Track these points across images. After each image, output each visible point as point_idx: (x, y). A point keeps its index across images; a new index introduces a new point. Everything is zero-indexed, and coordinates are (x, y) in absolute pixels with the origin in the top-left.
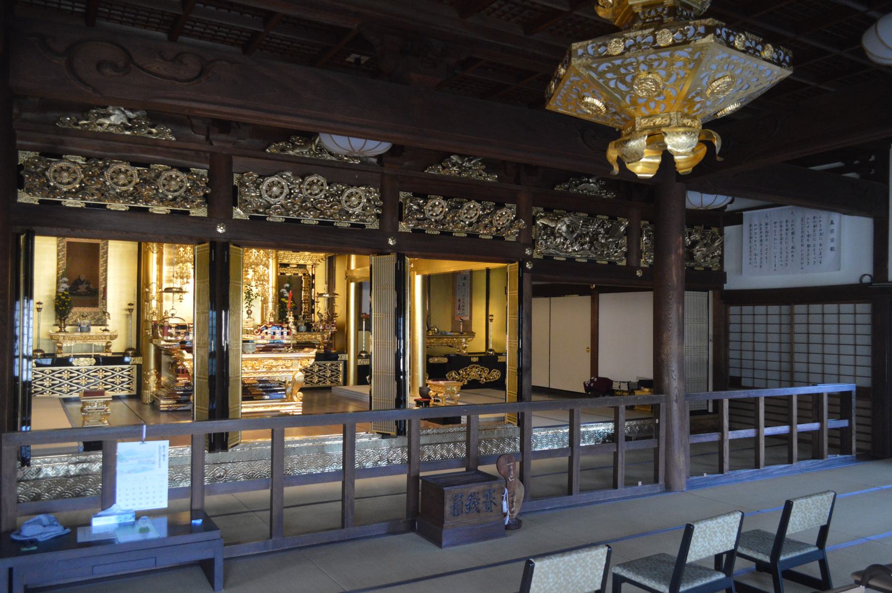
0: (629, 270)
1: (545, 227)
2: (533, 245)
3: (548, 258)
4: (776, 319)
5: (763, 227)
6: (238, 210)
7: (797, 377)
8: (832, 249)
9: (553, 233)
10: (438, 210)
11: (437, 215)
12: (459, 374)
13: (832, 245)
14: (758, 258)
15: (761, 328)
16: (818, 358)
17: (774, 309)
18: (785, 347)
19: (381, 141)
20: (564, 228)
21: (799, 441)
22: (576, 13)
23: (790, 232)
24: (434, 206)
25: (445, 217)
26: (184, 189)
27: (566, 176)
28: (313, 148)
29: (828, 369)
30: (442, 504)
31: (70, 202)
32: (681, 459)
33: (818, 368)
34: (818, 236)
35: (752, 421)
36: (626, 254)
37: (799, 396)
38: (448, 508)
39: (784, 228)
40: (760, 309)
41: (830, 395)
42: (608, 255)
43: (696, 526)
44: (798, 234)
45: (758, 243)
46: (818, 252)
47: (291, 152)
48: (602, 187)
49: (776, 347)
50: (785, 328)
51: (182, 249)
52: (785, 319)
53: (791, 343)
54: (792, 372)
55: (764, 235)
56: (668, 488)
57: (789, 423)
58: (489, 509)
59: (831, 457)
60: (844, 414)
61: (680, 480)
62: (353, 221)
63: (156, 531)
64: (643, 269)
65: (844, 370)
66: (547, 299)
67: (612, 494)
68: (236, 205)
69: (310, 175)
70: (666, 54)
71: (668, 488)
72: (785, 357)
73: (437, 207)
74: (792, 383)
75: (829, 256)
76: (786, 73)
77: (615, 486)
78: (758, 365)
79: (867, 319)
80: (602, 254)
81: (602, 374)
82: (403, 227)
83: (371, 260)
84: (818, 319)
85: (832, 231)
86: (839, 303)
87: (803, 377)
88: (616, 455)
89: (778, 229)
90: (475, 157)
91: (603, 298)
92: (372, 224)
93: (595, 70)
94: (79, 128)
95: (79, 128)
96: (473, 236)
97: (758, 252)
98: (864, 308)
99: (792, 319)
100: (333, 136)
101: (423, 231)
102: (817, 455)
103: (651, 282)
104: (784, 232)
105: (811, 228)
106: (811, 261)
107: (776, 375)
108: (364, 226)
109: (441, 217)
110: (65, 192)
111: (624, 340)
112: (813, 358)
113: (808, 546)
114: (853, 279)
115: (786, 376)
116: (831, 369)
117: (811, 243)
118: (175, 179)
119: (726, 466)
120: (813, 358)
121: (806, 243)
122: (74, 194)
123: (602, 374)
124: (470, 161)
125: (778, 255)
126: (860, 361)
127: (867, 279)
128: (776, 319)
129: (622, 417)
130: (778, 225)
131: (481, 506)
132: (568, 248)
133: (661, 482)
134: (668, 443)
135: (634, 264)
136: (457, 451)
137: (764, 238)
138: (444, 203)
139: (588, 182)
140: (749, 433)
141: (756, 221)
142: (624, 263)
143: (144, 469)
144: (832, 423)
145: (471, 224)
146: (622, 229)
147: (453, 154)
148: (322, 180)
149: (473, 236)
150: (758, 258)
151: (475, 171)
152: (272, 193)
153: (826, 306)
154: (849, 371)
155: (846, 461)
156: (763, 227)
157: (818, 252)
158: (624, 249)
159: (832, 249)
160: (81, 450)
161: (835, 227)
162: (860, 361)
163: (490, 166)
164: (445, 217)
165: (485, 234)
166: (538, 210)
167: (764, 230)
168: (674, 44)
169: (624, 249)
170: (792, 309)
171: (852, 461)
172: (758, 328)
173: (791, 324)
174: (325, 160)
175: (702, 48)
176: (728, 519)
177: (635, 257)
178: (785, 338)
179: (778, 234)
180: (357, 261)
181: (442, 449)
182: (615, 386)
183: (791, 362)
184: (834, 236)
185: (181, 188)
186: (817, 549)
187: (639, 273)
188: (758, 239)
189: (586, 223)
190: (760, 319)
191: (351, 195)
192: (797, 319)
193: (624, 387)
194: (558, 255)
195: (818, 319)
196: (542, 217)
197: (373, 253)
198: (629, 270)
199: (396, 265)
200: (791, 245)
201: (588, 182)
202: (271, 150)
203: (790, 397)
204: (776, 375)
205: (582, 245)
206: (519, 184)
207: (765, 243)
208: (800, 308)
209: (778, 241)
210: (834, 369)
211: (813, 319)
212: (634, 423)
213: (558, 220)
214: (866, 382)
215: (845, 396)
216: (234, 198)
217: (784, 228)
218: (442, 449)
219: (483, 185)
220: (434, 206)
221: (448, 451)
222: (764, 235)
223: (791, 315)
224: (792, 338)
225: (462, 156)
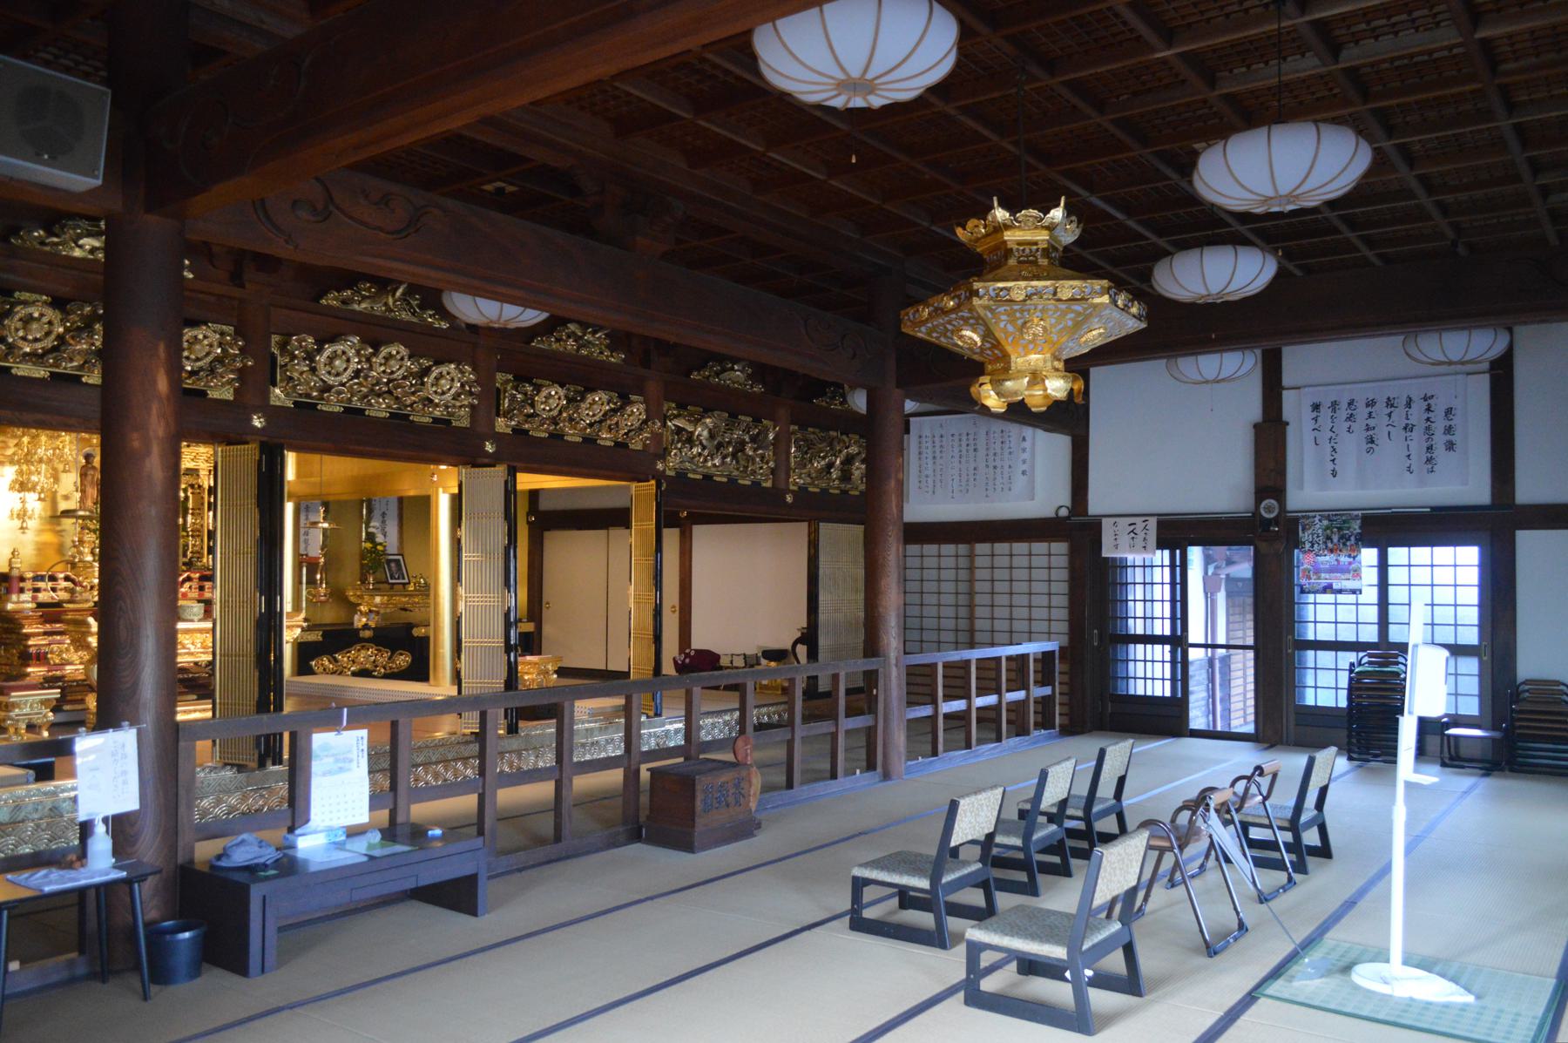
0: (776, 494)
1: (679, 430)
2: (663, 455)
3: (681, 475)
4: (951, 562)
5: (937, 439)
6: (277, 391)
7: (978, 637)
8: (1024, 473)
9: (690, 440)
10: (553, 403)
11: (198, 359)
12: (336, 660)
13: (1024, 467)
14: (930, 480)
15: (1021, 574)
16: (1005, 612)
17: (948, 549)
18: (963, 600)
19: (526, 306)
20: (705, 433)
21: (979, 720)
22: (833, 182)
23: (971, 448)
24: (549, 396)
25: (560, 413)
26: (53, 336)
27: (705, 358)
28: (391, 301)
29: (1017, 626)
30: (693, 797)
31: (23, 370)
32: (899, 738)
33: (1005, 625)
34: (1006, 455)
35: (993, 684)
36: (773, 471)
37: (946, 666)
38: (699, 804)
39: (964, 443)
40: (1020, 547)
41: (1009, 658)
42: (753, 472)
43: (962, 802)
44: (982, 452)
45: (930, 461)
46: (1006, 476)
47: (356, 307)
48: (749, 377)
49: (950, 599)
50: (963, 575)
51: (26, 439)
52: (963, 562)
53: (971, 594)
54: (972, 631)
55: (938, 449)
56: (886, 776)
57: (998, 691)
58: (738, 803)
59: (1036, 733)
60: (1046, 679)
61: (899, 762)
62: (437, 413)
63: (357, 851)
64: (793, 492)
65: (1036, 626)
66: (603, 532)
67: (834, 786)
68: (275, 385)
69: (388, 342)
70: (1063, 306)
71: (886, 776)
72: (963, 612)
73: (552, 398)
74: (972, 645)
75: (1020, 482)
76: (1143, 325)
77: (834, 776)
78: (927, 623)
79: (1063, 561)
80: (745, 471)
81: (698, 643)
82: (501, 425)
83: (459, 474)
84: (1005, 561)
85: (1024, 450)
86: (1409, 546)
87: (986, 637)
88: (790, 745)
89: (956, 444)
90: (601, 328)
91: (699, 531)
92: (462, 420)
93: (991, 311)
94: (47, 249)
95: (47, 249)
96: (589, 441)
97: (930, 472)
98: (1060, 548)
99: (972, 562)
100: (478, 299)
101: (526, 432)
102: (1021, 730)
103: (814, 509)
104: (964, 448)
105: (998, 445)
106: (999, 487)
107: (950, 637)
108: (449, 422)
109: (555, 413)
110: (26, 354)
111: (746, 589)
112: (998, 612)
113: (1107, 800)
114: (1048, 512)
115: (963, 637)
116: (1020, 626)
117: (998, 463)
118: (38, 320)
119: (941, 747)
120: (998, 612)
121: (991, 464)
122: (36, 358)
123: (698, 643)
124: (594, 333)
125: (957, 478)
126: (1056, 614)
127: (1064, 512)
128: (951, 562)
129: (751, 699)
130: (956, 438)
131: (731, 799)
132: (706, 461)
133: (879, 769)
134: (886, 720)
135: (782, 486)
136: (469, 772)
137: (938, 454)
138: (562, 392)
139: (732, 369)
140: (926, 711)
141: (927, 432)
142: (768, 484)
143: (341, 770)
144: (1039, 692)
145: (591, 425)
146: (771, 436)
147: (571, 321)
148: (404, 351)
149: (589, 441)
150: (930, 480)
151: (596, 347)
152: (338, 369)
153: (1015, 545)
154: (1043, 626)
155: (1050, 737)
156: (937, 439)
157: (1006, 476)
158: (772, 464)
159: (1024, 473)
160: (32, 779)
161: (1027, 445)
162: (1056, 614)
163: (617, 340)
164: (560, 413)
165: (572, 435)
166: (670, 407)
167: (938, 444)
168: (1072, 300)
169: (772, 464)
170: (972, 550)
171: (1055, 737)
172: (927, 574)
173: (971, 569)
174: (401, 321)
175: (1096, 306)
176: (989, 793)
177: (783, 476)
178: (963, 587)
179: (956, 450)
180: (299, 464)
181: (446, 770)
182: (724, 662)
183: (971, 618)
184: (1025, 456)
185: (48, 334)
186: (980, 865)
187: (789, 499)
188: (930, 456)
189: (729, 429)
190: (931, 562)
191: (441, 376)
192: (979, 562)
193: (739, 662)
194: (694, 472)
195: (1024, 561)
196: (676, 417)
197: (465, 464)
198: (776, 494)
199: (260, 462)
200: (972, 465)
201: (732, 369)
202: (331, 300)
203: (968, 662)
204: (950, 637)
205: (724, 457)
206: (242, 286)
207: (938, 461)
208: (982, 548)
209: (956, 459)
210: (1023, 626)
211: (1017, 561)
212: (772, 709)
213: (696, 422)
214: (1065, 640)
215: (1047, 657)
216: (270, 373)
217: (964, 443)
218: (446, 770)
219: (603, 366)
220: (549, 396)
221: (436, 776)
222: (938, 449)
223: (971, 556)
224: (972, 587)
225: (584, 325)
